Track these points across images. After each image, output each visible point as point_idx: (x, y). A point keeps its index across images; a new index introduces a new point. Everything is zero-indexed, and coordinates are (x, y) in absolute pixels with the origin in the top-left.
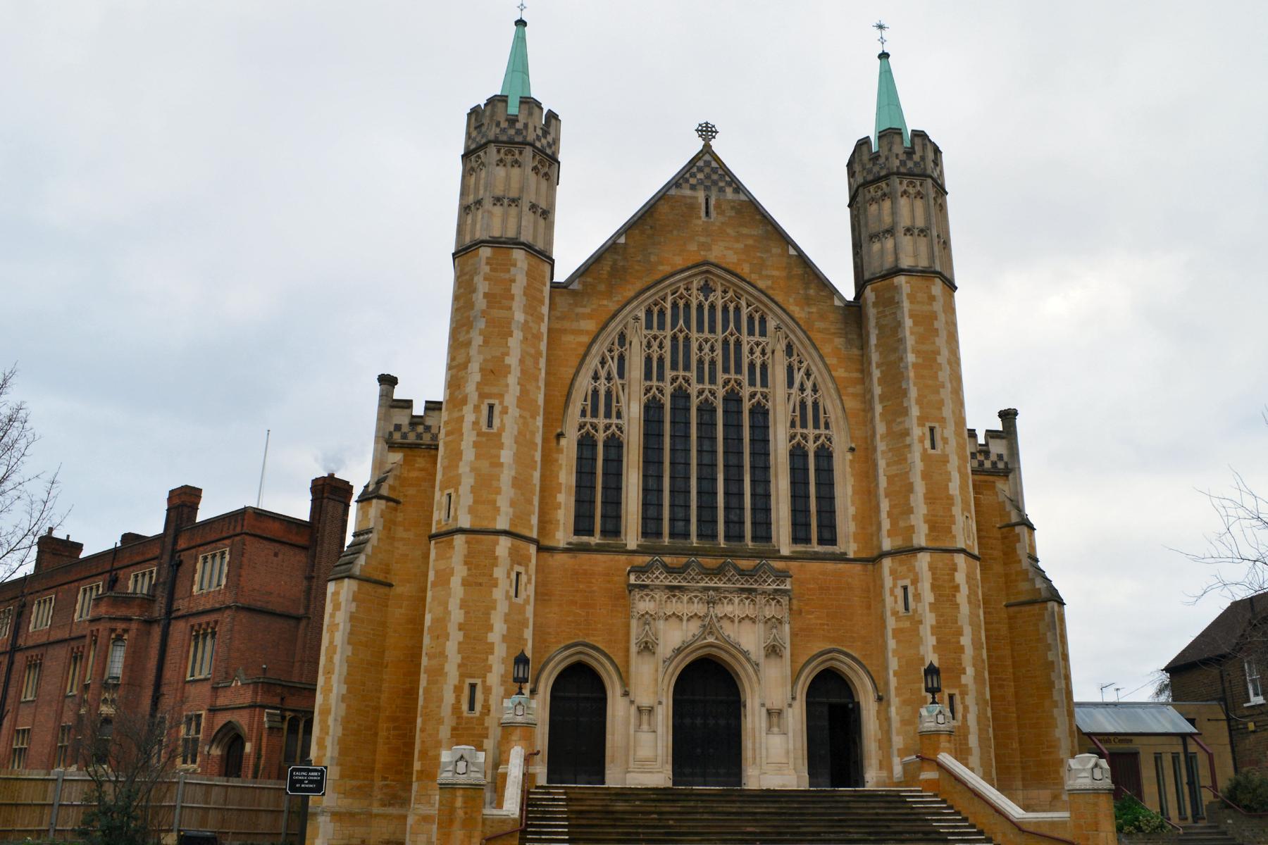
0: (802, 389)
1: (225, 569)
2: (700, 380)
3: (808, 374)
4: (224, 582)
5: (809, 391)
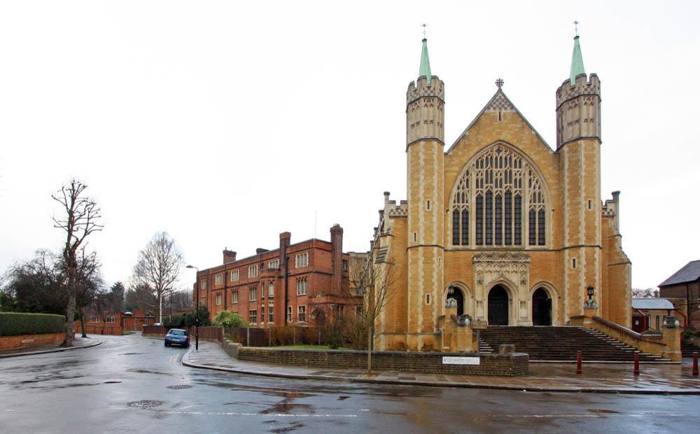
0: (534, 188)
1: (308, 260)
2: (496, 187)
3: (537, 182)
4: (308, 264)
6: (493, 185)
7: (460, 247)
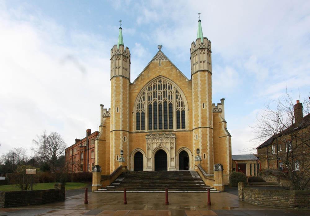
5: (180, 99)
6: (157, 99)
7: (181, 129)
